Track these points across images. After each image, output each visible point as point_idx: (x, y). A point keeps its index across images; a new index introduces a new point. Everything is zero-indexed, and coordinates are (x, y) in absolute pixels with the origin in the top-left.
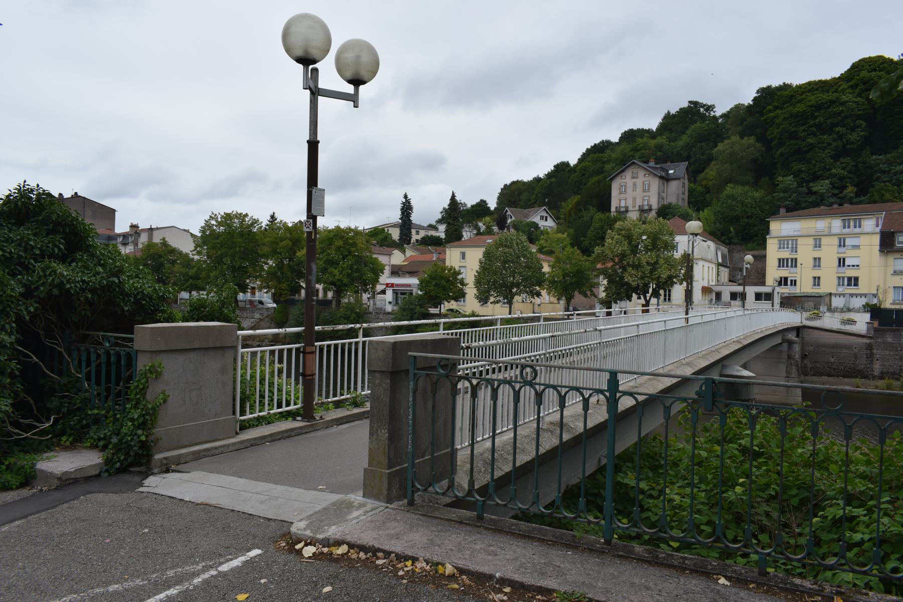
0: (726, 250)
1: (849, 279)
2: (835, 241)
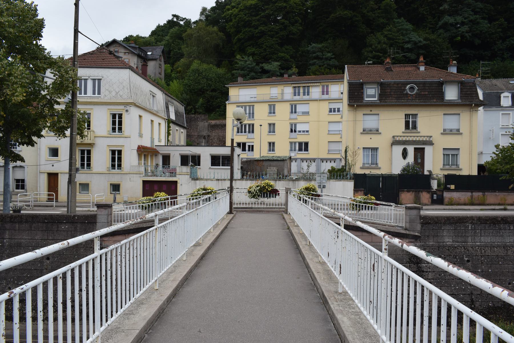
0: (182, 109)
1: (300, 144)
2: (287, 107)
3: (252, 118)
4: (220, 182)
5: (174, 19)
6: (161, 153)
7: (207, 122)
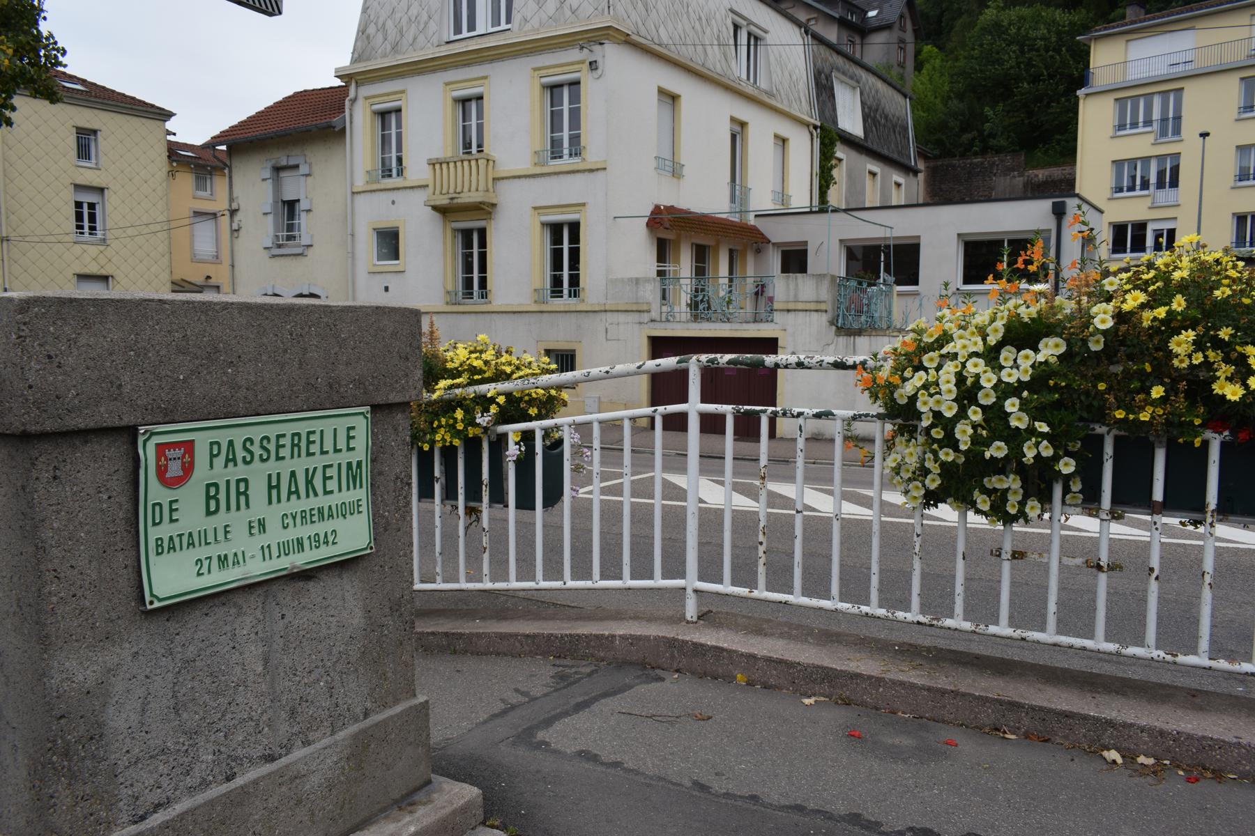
3: (1174, 134)
6: (773, 241)
7: (1021, 175)
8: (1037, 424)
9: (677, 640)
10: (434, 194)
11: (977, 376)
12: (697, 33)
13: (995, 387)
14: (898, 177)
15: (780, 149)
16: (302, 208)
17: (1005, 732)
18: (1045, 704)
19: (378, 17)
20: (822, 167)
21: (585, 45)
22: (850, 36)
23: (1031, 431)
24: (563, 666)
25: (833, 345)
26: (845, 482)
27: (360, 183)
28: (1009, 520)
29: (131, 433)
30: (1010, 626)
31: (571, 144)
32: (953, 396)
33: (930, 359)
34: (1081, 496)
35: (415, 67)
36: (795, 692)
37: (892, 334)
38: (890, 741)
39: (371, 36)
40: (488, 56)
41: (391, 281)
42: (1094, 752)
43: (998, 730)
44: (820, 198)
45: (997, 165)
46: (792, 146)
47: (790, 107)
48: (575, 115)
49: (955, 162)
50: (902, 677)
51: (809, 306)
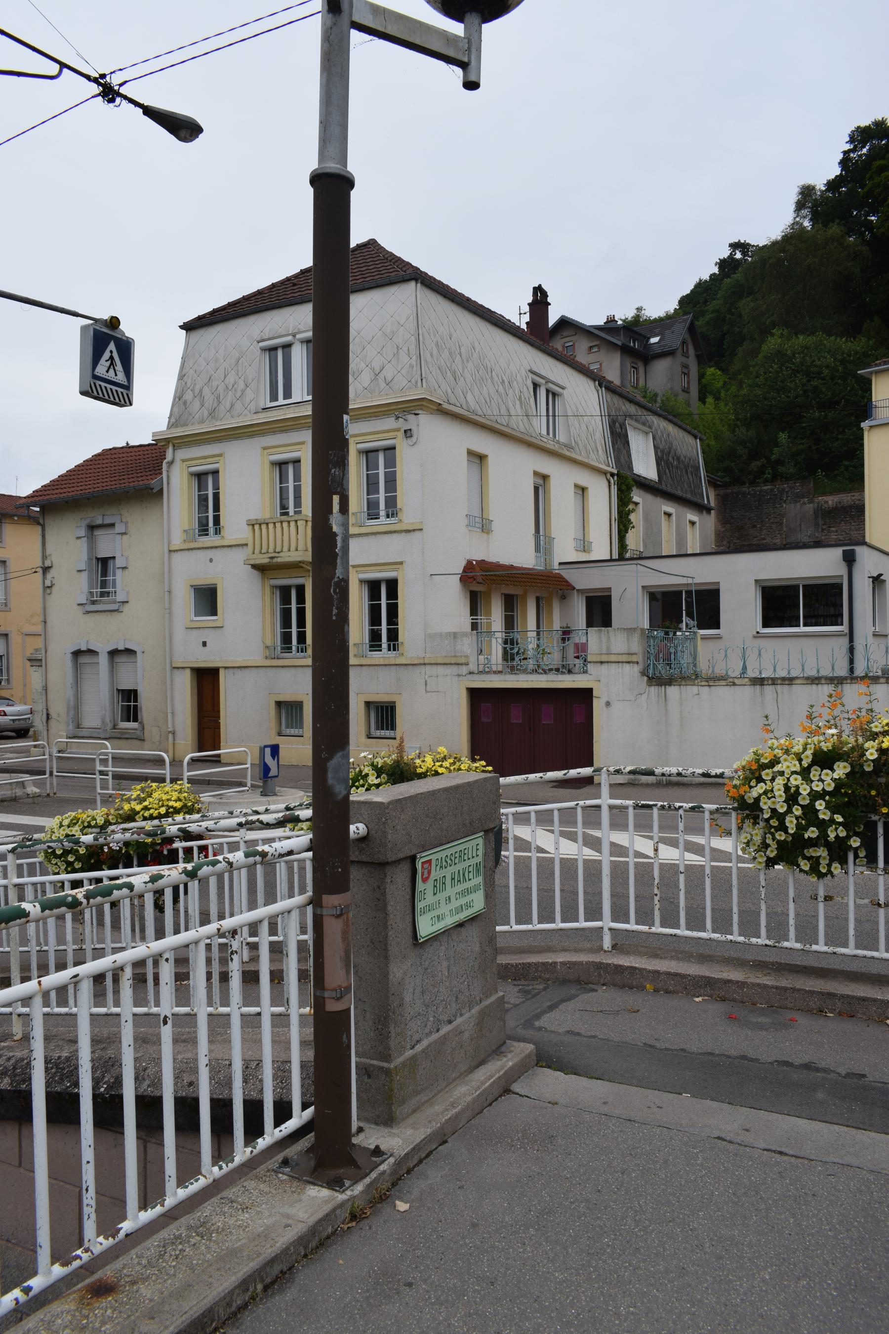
4: (769, 690)
5: (735, 254)
7: (811, 501)
8: (835, 816)
9: (603, 963)
10: (254, 553)
11: (797, 787)
12: (501, 396)
13: (809, 795)
14: (692, 516)
15: (580, 497)
16: (117, 566)
17: (826, 1013)
18: (850, 993)
19: (195, 385)
20: (620, 513)
21: (400, 416)
22: (633, 362)
23: (832, 821)
24: (522, 985)
25: (646, 694)
26: (661, 828)
27: (177, 541)
28: (821, 876)
29: (413, 859)
30: (826, 944)
31: (387, 507)
32: (784, 799)
33: (766, 774)
34: (865, 860)
35: (233, 433)
36: (687, 994)
37: (700, 684)
38: (755, 1020)
39: (188, 403)
40: (305, 423)
41: (210, 637)
42: (881, 1021)
43: (821, 1011)
44: (619, 542)
45: (787, 492)
46: (591, 494)
47: (588, 457)
48: (391, 482)
49: (745, 489)
50: (758, 981)
51: (620, 658)
